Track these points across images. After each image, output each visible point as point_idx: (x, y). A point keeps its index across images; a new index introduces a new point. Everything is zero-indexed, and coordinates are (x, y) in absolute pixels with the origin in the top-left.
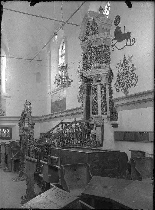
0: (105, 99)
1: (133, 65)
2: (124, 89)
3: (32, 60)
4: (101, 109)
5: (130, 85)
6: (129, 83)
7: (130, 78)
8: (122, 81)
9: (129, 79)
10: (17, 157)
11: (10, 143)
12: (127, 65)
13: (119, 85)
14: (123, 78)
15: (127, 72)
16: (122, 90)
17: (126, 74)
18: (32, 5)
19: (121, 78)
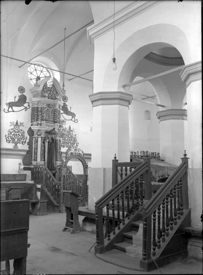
0: (45, 147)
1: (75, 135)
2: (68, 147)
3: (26, 63)
4: (38, 156)
5: (73, 146)
6: (72, 145)
7: (21, 137)
8: (67, 141)
9: (72, 142)
10: (155, 261)
11: (47, 203)
12: (71, 133)
13: (65, 144)
14: (67, 140)
15: (71, 137)
16: (66, 147)
17: (71, 138)
18: (53, 2)
19: (66, 139)
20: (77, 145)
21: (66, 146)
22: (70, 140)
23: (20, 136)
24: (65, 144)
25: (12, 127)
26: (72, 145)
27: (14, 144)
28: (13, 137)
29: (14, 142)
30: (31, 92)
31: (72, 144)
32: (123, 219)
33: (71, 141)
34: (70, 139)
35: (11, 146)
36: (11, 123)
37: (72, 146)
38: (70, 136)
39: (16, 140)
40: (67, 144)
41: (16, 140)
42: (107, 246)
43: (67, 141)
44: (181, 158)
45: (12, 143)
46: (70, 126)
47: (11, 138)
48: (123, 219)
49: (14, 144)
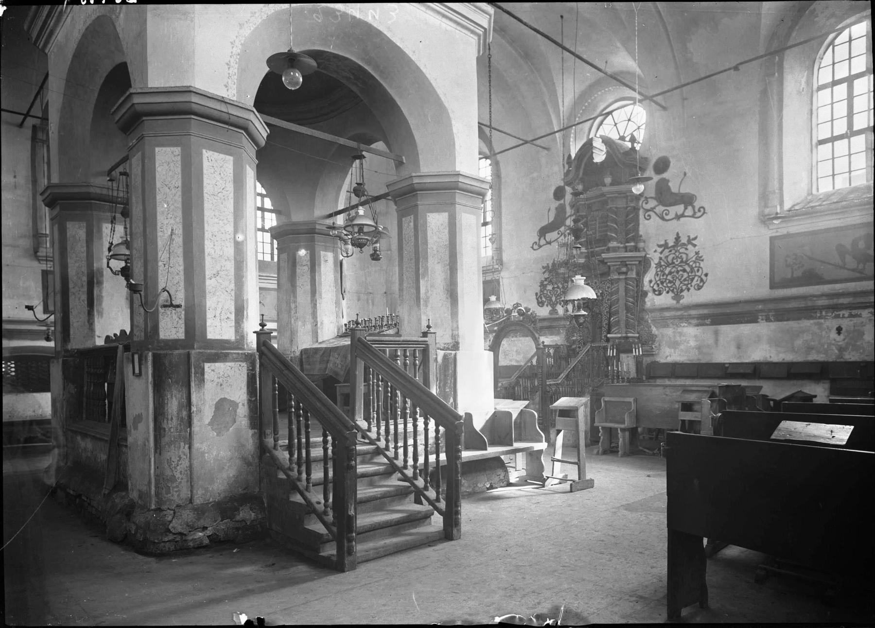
2: (673, 291)
6: (686, 282)
9: (685, 275)
14: (670, 273)
15: (682, 262)
16: (668, 292)
20: (702, 280)
21: (667, 289)
22: (678, 272)
23: (560, 290)
24: (665, 285)
25: (546, 275)
26: (686, 282)
27: (550, 308)
28: (549, 293)
29: (550, 303)
30: (260, 276)
31: (685, 280)
32: (56, 372)
33: (681, 273)
34: (679, 268)
35: (665, 300)
36: (543, 267)
37: (684, 287)
38: (679, 260)
39: (554, 299)
40: (669, 285)
41: (554, 299)
42: (394, 463)
43: (669, 277)
44: (254, 332)
45: (547, 306)
46: (678, 234)
47: (545, 297)
48: (56, 372)
49: (550, 308)
